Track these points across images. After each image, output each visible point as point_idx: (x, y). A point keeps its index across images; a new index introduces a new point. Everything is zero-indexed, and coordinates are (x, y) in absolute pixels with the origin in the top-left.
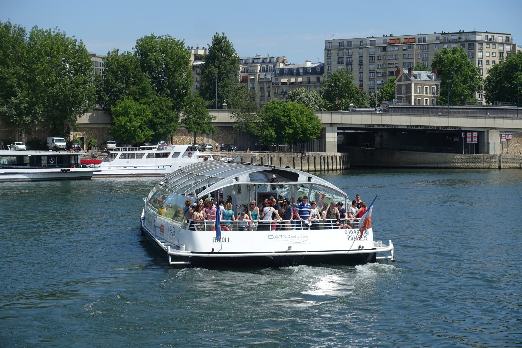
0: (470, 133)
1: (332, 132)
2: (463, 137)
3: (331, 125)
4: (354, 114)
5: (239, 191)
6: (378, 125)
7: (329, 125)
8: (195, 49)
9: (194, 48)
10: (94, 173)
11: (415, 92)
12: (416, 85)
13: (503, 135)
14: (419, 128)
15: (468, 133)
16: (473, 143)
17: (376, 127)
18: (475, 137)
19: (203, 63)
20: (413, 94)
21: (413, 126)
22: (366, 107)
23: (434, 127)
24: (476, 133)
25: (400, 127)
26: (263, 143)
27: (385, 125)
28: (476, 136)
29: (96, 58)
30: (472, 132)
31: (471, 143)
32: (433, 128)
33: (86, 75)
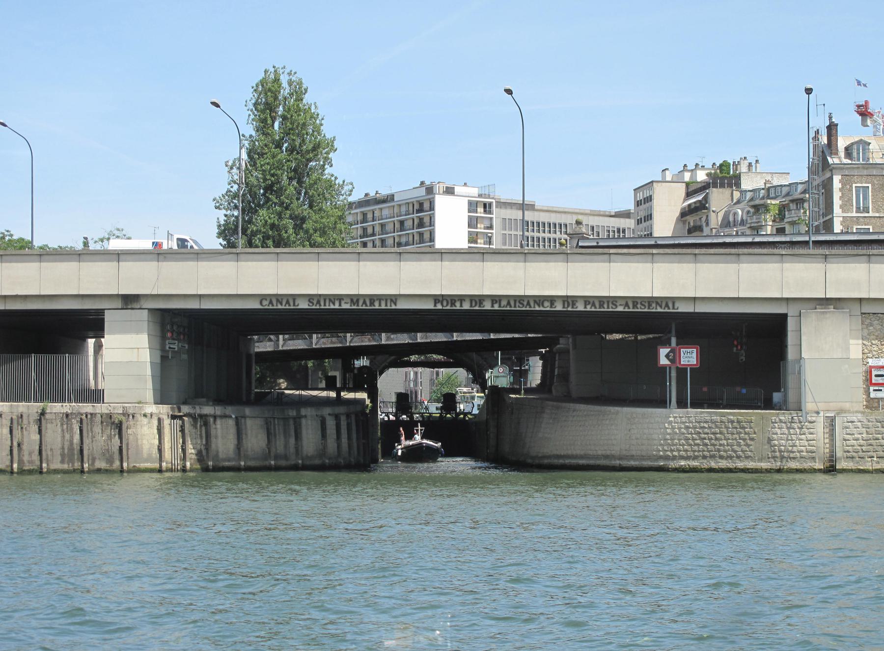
2: (664, 368)
3: (129, 301)
4: (491, 261)
5: (86, 416)
6: (310, 298)
7: (119, 304)
8: (692, 170)
9: (689, 168)
11: (844, 207)
14: (487, 306)
17: (303, 305)
21: (461, 298)
22: (257, 247)
23: (552, 299)
25: (402, 305)
27: (340, 298)
29: (536, 213)
32: (547, 307)
33: (336, 239)
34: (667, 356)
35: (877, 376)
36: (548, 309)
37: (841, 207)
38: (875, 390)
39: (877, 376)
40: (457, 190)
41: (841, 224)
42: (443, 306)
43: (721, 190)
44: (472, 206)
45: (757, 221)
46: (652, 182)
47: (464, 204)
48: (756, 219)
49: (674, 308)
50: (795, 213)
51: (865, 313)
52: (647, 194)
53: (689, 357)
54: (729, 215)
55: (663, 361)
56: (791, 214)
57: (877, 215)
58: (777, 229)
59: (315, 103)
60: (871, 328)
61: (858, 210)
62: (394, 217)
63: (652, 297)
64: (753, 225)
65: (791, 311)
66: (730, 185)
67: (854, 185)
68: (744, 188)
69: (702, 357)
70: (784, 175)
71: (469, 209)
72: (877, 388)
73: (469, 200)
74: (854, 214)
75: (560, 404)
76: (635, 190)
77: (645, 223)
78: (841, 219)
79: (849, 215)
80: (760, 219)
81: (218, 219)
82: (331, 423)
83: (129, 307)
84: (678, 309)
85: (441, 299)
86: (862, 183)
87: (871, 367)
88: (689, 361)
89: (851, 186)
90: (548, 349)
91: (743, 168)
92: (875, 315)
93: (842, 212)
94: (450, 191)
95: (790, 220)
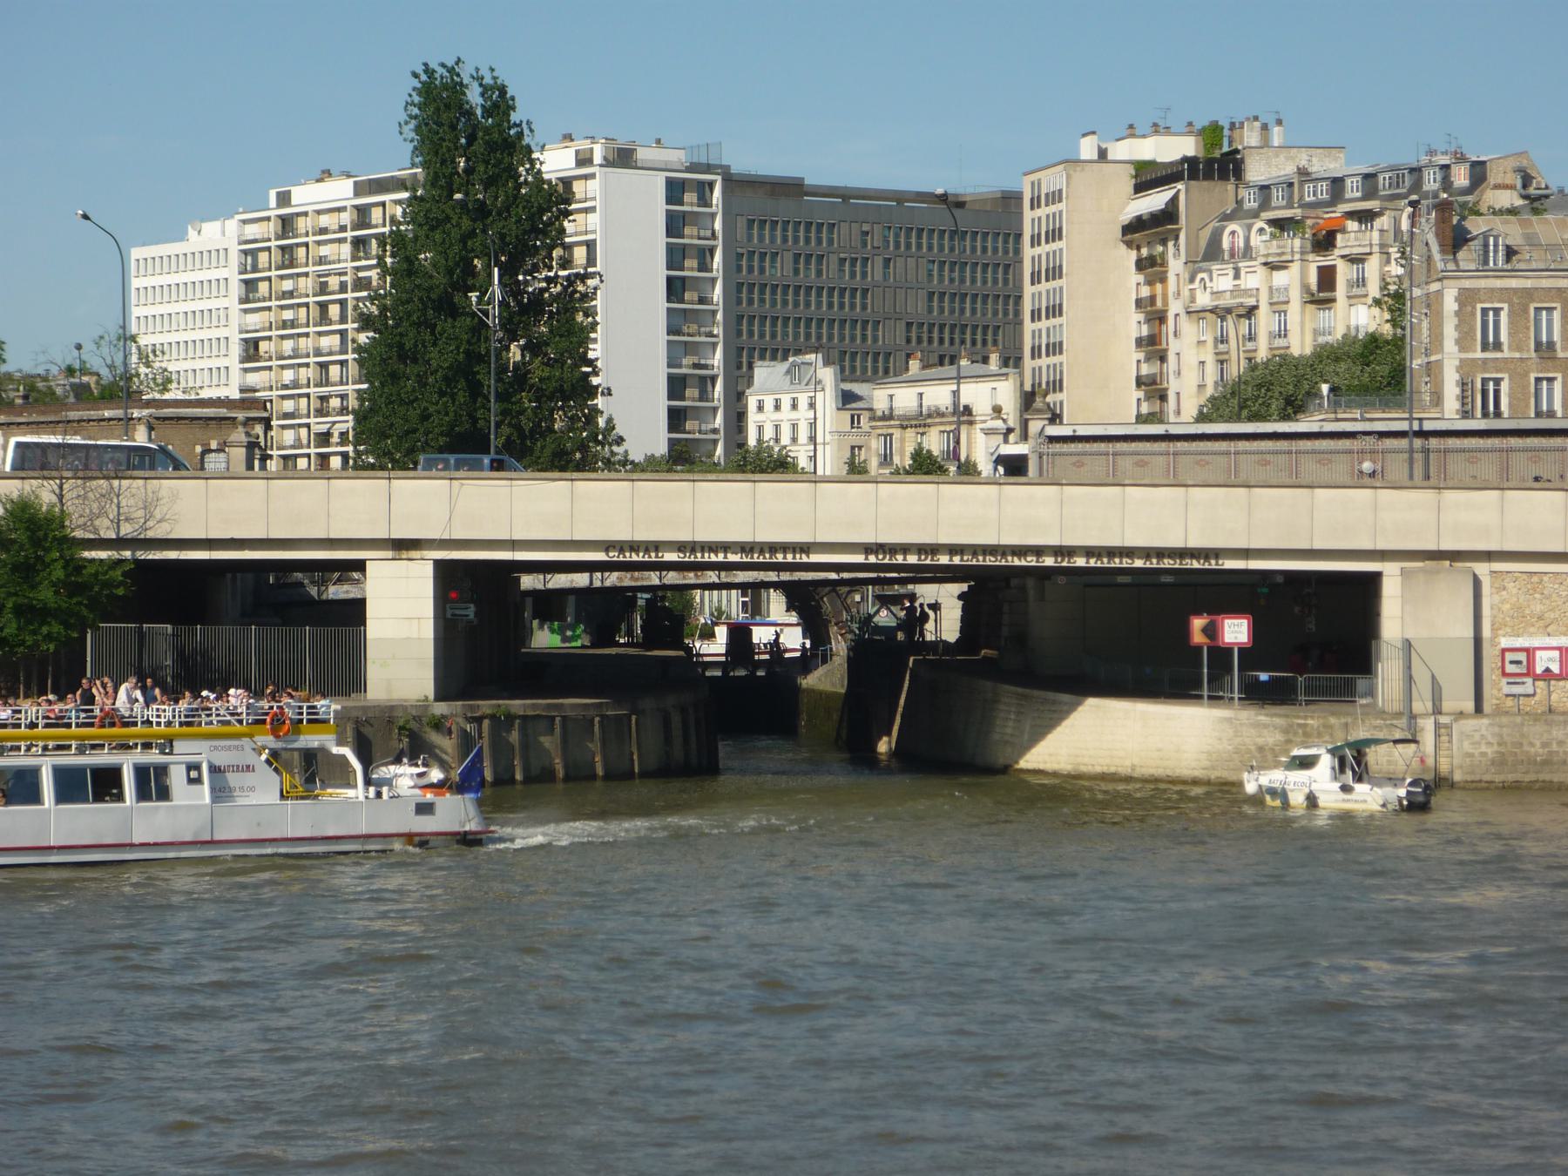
2: (1199, 648)
3: (402, 546)
10: (528, 582)
11: (1463, 343)
12: (1466, 298)
20: (1450, 345)
32: (1031, 561)
35: (1512, 662)
37: (1458, 342)
38: (1508, 683)
39: (1512, 662)
40: (642, 154)
41: (1458, 372)
43: (1205, 183)
44: (675, 190)
45: (1279, 251)
47: (658, 182)
48: (1279, 247)
50: (1356, 239)
51: (1495, 572)
53: (1236, 631)
54: (1221, 235)
56: (1348, 240)
57: (1517, 355)
58: (1319, 267)
59: (529, 123)
60: (1504, 593)
61: (1485, 348)
63: (1186, 549)
64: (1270, 259)
66: (1224, 176)
67: (1479, 306)
68: (1251, 179)
69: (1255, 631)
70: (1334, 151)
72: (1512, 680)
73: (667, 178)
74: (1479, 355)
75: (1027, 691)
77: (1048, 246)
78: (1457, 363)
79: (1470, 355)
80: (1284, 247)
82: (676, 720)
83: (404, 557)
85: (875, 548)
86: (1492, 302)
87: (1504, 651)
88: (1236, 638)
89: (1474, 308)
90: (973, 583)
91: (1251, 137)
93: (1460, 351)
95: (1346, 252)
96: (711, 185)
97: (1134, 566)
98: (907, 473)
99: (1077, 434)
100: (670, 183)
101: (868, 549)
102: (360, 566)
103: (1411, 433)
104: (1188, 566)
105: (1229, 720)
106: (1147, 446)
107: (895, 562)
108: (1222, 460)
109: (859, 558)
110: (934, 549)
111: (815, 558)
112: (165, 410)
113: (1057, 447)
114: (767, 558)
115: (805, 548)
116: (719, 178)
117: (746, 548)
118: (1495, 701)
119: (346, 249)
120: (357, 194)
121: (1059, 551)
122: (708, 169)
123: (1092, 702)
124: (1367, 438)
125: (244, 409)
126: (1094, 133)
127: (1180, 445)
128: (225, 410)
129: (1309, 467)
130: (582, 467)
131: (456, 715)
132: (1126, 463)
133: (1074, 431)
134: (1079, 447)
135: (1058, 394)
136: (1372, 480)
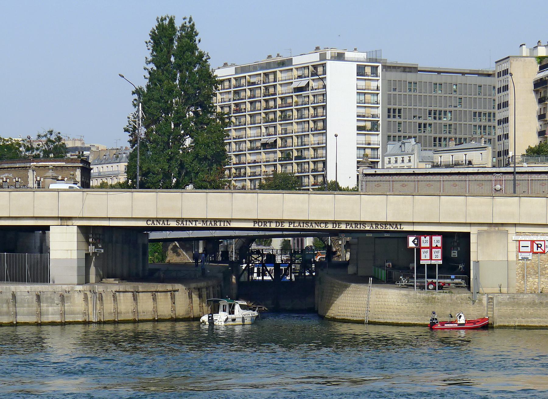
0: (428, 238)
1: (272, 75)
2: (412, 249)
10: (154, 235)
13: (522, 244)
15: (423, 238)
16: (433, 262)
18: (437, 247)
19: (94, 257)
24: (439, 238)
26: (301, 259)
28: (439, 245)
30: (431, 234)
31: (429, 262)
32: (323, 226)
34: (413, 242)
36: (324, 228)
42: (259, 226)
46: (509, 57)
47: (353, 67)
49: (400, 229)
52: (504, 66)
55: (411, 245)
62: (292, 79)
63: (386, 222)
65: (473, 231)
71: (357, 73)
73: (357, 65)
76: (496, 62)
81: (144, 76)
83: (65, 224)
84: (403, 229)
92: (524, 234)
94: (340, 57)
96: (377, 67)
97: (365, 229)
98: (99, 188)
99: (376, 173)
100: (359, 67)
101: (255, 221)
102: (47, 228)
103: (515, 173)
104: (388, 229)
105: (406, 295)
106: (406, 178)
107: (266, 227)
108: (438, 184)
109: (251, 225)
110: (282, 221)
111: (234, 225)
112: (40, 163)
113: (369, 178)
114: (213, 225)
115: (229, 221)
116: (380, 65)
117: (204, 220)
118: (517, 288)
119: (231, 96)
120: (236, 73)
121: (334, 222)
122: (376, 61)
123: (353, 285)
124: (498, 175)
125: (72, 163)
126: (524, 45)
127: (420, 177)
128: (65, 163)
129: (474, 187)
130: (217, 188)
131: (87, 291)
132: (397, 185)
133: (375, 172)
134: (378, 178)
135: (500, 157)
136: (497, 193)
